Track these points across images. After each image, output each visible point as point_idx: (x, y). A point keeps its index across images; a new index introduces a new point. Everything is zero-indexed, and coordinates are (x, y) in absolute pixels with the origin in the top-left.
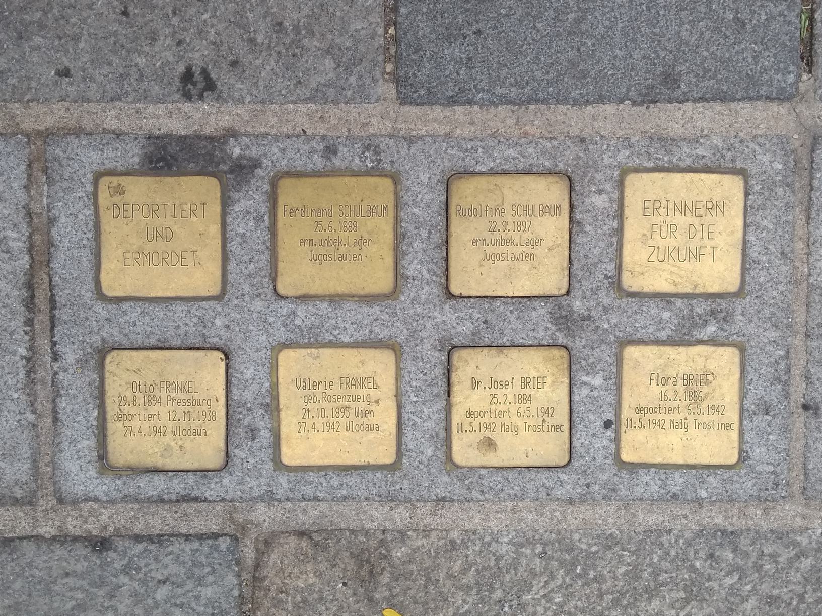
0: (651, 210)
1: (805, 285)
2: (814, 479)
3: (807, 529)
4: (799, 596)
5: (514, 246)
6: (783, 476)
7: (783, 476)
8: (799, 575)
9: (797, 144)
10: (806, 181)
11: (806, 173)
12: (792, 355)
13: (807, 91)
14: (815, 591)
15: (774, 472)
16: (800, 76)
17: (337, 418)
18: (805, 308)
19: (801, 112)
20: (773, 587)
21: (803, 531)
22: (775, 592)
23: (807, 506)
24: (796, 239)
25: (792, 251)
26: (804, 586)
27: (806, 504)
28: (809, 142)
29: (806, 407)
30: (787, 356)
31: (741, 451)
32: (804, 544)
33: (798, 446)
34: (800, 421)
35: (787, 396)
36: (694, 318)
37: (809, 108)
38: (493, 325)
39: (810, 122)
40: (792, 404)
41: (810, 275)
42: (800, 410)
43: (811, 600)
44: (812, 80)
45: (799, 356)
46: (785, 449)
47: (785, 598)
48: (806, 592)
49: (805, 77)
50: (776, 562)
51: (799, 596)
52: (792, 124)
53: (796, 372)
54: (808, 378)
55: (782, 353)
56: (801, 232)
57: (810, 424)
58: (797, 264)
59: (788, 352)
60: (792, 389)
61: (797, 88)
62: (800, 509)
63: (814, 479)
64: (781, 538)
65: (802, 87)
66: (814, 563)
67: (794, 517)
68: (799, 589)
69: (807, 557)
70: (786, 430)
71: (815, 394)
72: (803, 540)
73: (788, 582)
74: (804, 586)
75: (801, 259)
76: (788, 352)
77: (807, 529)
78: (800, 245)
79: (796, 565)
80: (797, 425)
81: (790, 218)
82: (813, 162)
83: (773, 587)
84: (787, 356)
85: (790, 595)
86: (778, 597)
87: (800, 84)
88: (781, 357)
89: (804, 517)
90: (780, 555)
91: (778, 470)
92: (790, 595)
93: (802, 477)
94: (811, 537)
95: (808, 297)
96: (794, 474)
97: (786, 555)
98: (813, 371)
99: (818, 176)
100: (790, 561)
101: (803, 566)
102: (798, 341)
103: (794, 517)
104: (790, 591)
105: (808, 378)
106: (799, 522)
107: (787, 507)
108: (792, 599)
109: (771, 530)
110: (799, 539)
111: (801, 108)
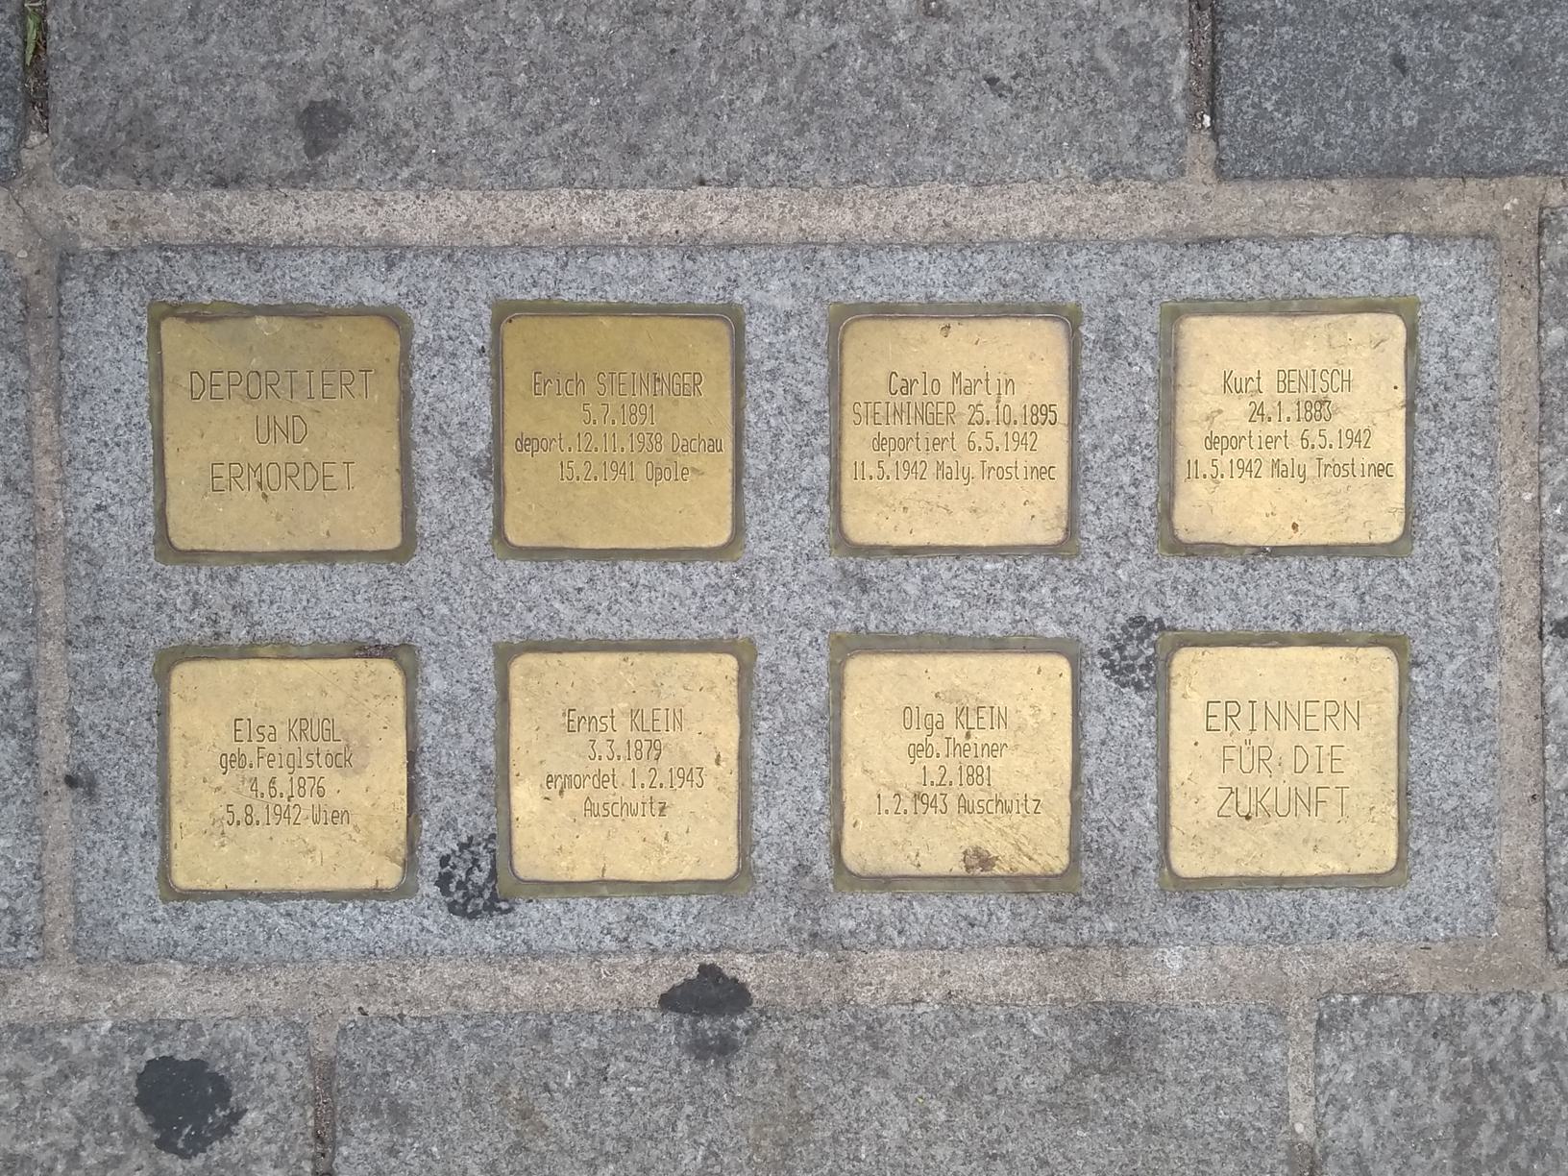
0: (224, 386)
1: (60, 542)
2: (90, 922)
3: (82, 1020)
4: (68, 1153)
5: (966, 436)
6: (28, 918)
7: (28, 918)
8: (66, 1112)
9: (28, 269)
10: (50, 341)
11: (51, 325)
12: (39, 675)
13: (39, 165)
14: (99, 1143)
15: (11, 911)
16: (25, 137)
17: (626, 790)
18: (61, 587)
19: (34, 206)
20: (17, 1137)
21: (74, 1024)
22: (22, 1147)
23: (83, 975)
24: (37, 453)
25: (30, 478)
26: (79, 1134)
27: (81, 971)
28: (52, 265)
29: (71, 781)
30: (28, 680)
31: (1212, 883)
32: (75, 1051)
33: (59, 857)
34: (62, 809)
35: (31, 759)
36: (1296, 593)
37: (46, 198)
38: (887, 606)
39: (51, 226)
40: (44, 776)
41: (67, 523)
42: (63, 787)
43: (92, 1161)
44: (47, 146)
45: (55, 682)
46: (31, 865)
47: (42, 1158)
48: (81, 1146)
49: (35, 138)
50: (21, 1087)
51: (68, 1153)
52: (15, 231)
53: (50, 713)
54: (72, 721)
55: (15, 676)
56: (46, 440)
57: (80, 813)
58: (43, 502)
59: (28, 674)
60: (43, 746)
61: (18, 162)
62: (69, 982)
63: (90, 922)
64: (30, 1041)
65: (28, 157)
66: (95, 1087)
67: (58, 997)
68: (68, 1141)
69: (82, 1078)
70: (32, 826)
71: (86, 756)
72: (73, 1042)
73: (46, 1127)
74: (79, 1134)
75: (51, 492)
76: (28, 674)
77: (82, 1020)
78: (45, 465)
79: (61, 1092)
80: (56, 815)
81: (21, 412)
82: (60, 303)
83: (17, 1137)
84: (28, 680)
85: (50, 1153)
86: (27, 1158)
87: (25, 153)
88: (14, 685)
89: (76, 998)
90: (29, 1075)
91: (19, 905)
92: (50, 1153)
93: (70, 919)
94: (88, 1036)
95: (65, 567)
96: (54, 914)
97: (39, 1073)
98: (81, 710)
99: (70, 330)
100: (49, 1084)
101: (73, 1094)
102: (51, 651)
103: (58, 997)
104: (50, 1145)
105: (72, 721)
106: (67, 1008)
107: (43, 979)
108: (55, 1160)
109: (11, 1026)
110: (64, 1041)
111: (33, 198)
